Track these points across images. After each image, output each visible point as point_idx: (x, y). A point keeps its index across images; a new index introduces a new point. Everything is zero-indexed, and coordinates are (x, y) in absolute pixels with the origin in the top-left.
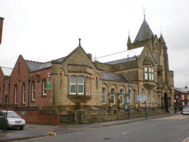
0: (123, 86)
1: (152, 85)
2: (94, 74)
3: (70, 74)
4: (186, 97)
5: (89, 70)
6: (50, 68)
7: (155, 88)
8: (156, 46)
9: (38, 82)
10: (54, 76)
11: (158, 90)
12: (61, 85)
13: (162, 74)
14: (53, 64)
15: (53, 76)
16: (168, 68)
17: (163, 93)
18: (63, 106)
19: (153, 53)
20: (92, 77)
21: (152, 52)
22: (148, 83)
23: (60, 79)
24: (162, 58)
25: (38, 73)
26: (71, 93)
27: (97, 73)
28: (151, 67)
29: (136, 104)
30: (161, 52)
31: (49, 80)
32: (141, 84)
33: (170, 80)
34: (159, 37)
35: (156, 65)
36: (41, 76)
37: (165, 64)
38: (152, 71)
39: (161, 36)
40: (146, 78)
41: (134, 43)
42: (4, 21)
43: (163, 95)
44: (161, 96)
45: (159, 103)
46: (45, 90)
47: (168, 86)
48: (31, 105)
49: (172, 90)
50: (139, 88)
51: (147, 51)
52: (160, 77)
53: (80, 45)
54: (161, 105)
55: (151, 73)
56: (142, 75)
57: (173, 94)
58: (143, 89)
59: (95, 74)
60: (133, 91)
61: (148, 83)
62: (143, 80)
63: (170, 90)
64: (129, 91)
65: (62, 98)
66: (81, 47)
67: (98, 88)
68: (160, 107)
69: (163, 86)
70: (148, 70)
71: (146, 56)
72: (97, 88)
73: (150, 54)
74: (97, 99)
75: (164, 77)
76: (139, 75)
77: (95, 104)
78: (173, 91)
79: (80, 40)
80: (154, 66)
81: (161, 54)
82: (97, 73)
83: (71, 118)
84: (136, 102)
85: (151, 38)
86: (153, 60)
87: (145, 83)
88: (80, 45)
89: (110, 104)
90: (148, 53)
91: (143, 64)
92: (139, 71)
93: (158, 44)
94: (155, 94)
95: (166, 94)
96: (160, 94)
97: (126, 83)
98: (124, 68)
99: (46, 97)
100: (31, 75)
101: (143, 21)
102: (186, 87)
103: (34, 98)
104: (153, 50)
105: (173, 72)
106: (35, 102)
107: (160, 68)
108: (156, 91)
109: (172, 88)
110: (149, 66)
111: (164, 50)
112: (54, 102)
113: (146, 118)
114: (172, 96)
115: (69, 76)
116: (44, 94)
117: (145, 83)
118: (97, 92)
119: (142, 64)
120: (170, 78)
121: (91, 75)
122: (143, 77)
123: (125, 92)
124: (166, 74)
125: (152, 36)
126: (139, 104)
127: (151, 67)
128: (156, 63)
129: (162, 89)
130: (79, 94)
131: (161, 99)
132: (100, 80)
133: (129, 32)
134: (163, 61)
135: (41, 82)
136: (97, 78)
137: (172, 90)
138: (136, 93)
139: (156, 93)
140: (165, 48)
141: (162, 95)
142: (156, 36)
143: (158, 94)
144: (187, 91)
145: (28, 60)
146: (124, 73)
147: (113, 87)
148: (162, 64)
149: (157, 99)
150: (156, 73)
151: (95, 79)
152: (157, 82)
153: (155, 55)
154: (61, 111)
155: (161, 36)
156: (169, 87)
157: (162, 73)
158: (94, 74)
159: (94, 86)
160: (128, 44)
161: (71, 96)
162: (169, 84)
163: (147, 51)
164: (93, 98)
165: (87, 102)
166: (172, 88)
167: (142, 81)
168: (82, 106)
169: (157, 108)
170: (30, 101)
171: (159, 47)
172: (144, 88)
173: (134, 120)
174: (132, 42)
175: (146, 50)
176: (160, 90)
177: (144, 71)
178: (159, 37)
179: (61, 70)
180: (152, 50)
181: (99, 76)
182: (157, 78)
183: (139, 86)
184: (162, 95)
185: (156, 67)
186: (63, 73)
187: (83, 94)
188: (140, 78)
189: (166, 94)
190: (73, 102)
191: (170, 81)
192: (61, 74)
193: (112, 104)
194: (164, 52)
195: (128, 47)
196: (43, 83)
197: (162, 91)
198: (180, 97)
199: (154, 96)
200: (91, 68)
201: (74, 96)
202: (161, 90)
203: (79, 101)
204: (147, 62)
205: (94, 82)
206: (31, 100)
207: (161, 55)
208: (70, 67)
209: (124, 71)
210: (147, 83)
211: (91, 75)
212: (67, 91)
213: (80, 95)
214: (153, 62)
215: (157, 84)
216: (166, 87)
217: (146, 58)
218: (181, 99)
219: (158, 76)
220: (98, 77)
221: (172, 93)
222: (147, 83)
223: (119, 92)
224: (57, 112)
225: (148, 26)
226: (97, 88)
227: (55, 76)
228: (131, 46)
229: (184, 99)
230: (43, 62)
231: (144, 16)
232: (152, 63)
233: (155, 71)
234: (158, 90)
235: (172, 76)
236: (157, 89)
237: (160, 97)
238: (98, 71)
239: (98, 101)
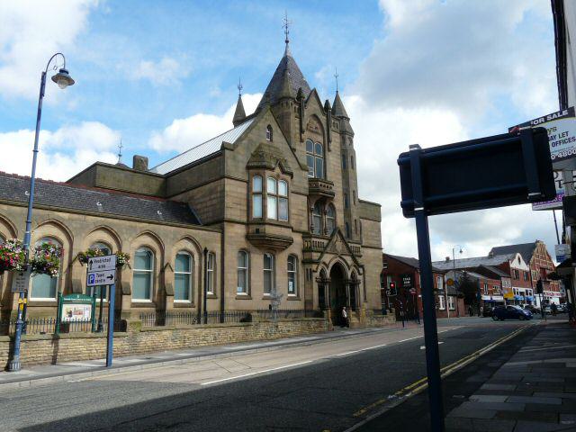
11: (307, 256)
13: (333, 208)
16: (355, 192)
17: (324, 263)
24: (334, 161)
28: (277, 179)
29: (208, 301)
30: (329, 141)
40: (257, 212)
43: (328, 272)
44: (317, 275)
50: (226, 245)
55: (276, 196)
56: (245, 203)
58: (243, 252)
60: (200, 255)
62: (245, 220)
68: (312, 311)
70: (264, 187)
76: (228, 201)
81: (332, 147)
84: (209, 293)
90: (270, 136)
91: (248, 168)
93: (323, 119)
97: (166, 225)
101: (281, 56)
104: (302, 131)
110: (268, 173)
117: (253, 228)
119: (242, 166)
120: (366, 223)
122: (245, 208)
127: (278, 176)
140: (346, 134)
142: (315, 93)
143: (308, 266)
145: (15, 173)
156: (347, 246)
163: (269, 127)
167: (243, 223)
169: (303, 314)
171: (325, 127)
177: (249, 189)
183: (226, 239)
188: (233, 211)
189: (338, 269)
197: (320, 258)
207: (329, 150)
210: (257, 231)
217: (260, 147)
222: (257, 231)
231: (287, 42)
234: (307, 256)
236: (304, 251)
237: (314, 280)
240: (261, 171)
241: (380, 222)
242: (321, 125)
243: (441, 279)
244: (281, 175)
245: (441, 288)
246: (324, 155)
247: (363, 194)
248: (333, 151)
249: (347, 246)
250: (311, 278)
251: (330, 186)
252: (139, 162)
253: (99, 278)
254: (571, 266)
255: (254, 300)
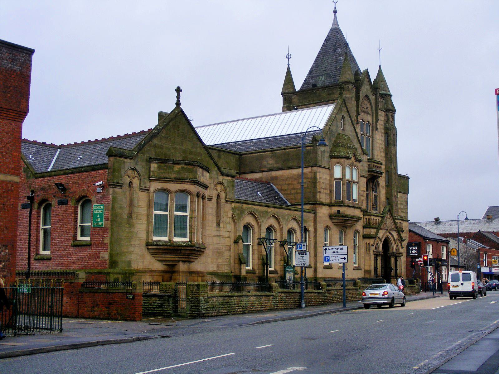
0: (274, 216)
1: (352, 217)
2: (212, 186)
3: (154, 186)
4: (437, 251)
5: (203, 175)
6: (101, 169)
7: (359, 226)
8: (366, 104)
9: (61, 203)
10: (113, 190)
11: (367, 231)
12: (130, 215)
14: (112, 159)
15: (111, 190)
16: (396, 168)
17: (379, 238)
18: (135, 270)
19: (358, 123)
20: (207, 193)
21: (353, 119)
22: (342, 210)
23: (128, 199)
24: (379, 139)
25: (63, 179)
26: (156, 238)
27: (221, 183)
28: (351, 166)
30: (377, 121)
31: (99, 202)
32: (323, 212)
33: (399, 202)
34: (373, 76)
35: (365, 158)
36: (73, 189)
37: (386, 154)
38: (355, 178)
39: (380, 73)
41: (301, 91)
42: (35, 57)
43: (381, 245)
44: (373, 248)
45: (367, 268)
46: (83, 228)
47: (394, 219)
48: (37, 267)
49: (403, 231)
50: (318, 225)
51: (343, 118)
52: (373, 194)
53: (178, 104)
54: (373, 273)
57: (405, 243)
58: (327, 228)
59: (215, 185)
61: (342, 210)
63: (399, 231)
64: (290, 232)
65: (131, 249)
66: (182, 111)
67: (222, 225)
69: (380, 219)
71: (338, 134)
72: (218, 224)
73: (349, 128)
74: (219, 253)
75: (382, 193)
77: (212, 268)
78: (405, 235)
79: (178, 90)
80: (360, 161)
81: (378, 126)
82: (221, 183)
83: (169, 302)
85: (354, 81)
86: (357, 145)
87: (335, 209)
88: (178, 104)
89: (240, 269)
91: (331, 157)
92: (318, 176)
93: (372, 98)
94: (359, 239)
95: (386, 243)
96: (371, 241)
98: (275, 166)
99: (87, 245)
100: (38, 183)
101: (329, 27)
102: (437, 221)
103: (45, 249)
104: (358, 114)
105: (407, 178)
106: (50, 259)
107: (375, 169)
108: (361, 233)
109: (405, 224)
110: (347, 161)
111: (387, 115)
112: (113, 264)
113: (434, 295)
114: (402, 248)
115: (152, 190)
116: (80, 238)
117: (335, 209)
118: (219, 236)
121: (206, 187)
122: (328, 192)
123: (278, 234)
124: (389, 185)
125: (357, 73)
126: (315, 271)
127: (353, 163)
128: (364, 153)
129: (377, 228)
130: (176, 239)
131: (373, 257)
132: (227, 201)
133: (289, 57)
134: (383, 147)
135: (71, 203)
136: (218, 196)
137: (403, 231)
138: (309, 238)
139: (361, 238)
140: (390, 111)
141: (377, 244)
142: (367, 73)
143: (367, 241)
144: (438, 233)
145: (35, 139)
146: (276, 178)
147: (249, 219)
148: (379, 156)
149: (362, 255)
150: (364, 181)
151: (214, 199)
152: (364, 206)
153: (362, 130)
154: (118, 282)
155: (380, 73)
156: (395, 223)
157: (378, 182)
158: (212, 186)
159: (211, 218)
160: (286, 91)
161: (156, 245)
162: (395, 216)
163: (343, 118)
164: (208, 252)
165: (192, 262)
166: (405, 224)
168: (183, 272)
170: (33, 256)
171: (374, 106)
172: (330, 223)
173: (316, 310)
174: (298, 86)
175: (339, 117)
176: (373, 231)
178: (373, 76)
179: (130, 173)
180: (354, 114)
181: (225, 193)
182: (365, 195)
183: (318, 219)
184: (377, 244)
185: (364, 166)
186: (136, 182)
187: (186, 239)
189: (386, 243)
190: (158, 260)
191: (399, 206)
192: (130, 184)
193: (247, 268)
194: (387, 121)
195: (285, 100)
196: (76, 208)
197: (377, 233)
198: (421, 251)
199: (355, 247)
200: (207, 170)
201: (163, 245)
202: (375, 230)
203: (177, 259)
204: (341, 149)
205: (211, 207)
206: (37, 254)
207: (377, 130)
208: (154, 166)
209: (274, 174)
210: (339, 211)
211: (206, 187)
212: (145, 232)
213: (180, 244)
214: (356, 149)
215: (365, 212)
216: (389, 220)
218: (425, 258)
219: (367, 190)
220: (223, 195)
221: (403, 240)
222: (339, 211)
223: (263, 235)
224: (138, 288)
225: (346, 45)
226: (218, 224)
227: (118, 190)
228: (295, 99)
229: (431, 257)
230: (58, 144)
231: (335, 12)
232: (354, 155)
233: (361, 176)
234: (367, 231)
235: (406, 191)
236: (364, 227)
238: (221, 178)
239: (220, 261)
240: (342, 160)
241: (408, 193)
242: (371, 105)
243: (445, 249)
244: (355, 163)
245: (444, 257)
246: (372, 134)
247: (401, 171)
248: (379, 130)
249: (395, 223)
250: (369, 250)
251: (379, 165)
252: (161, 115)
253: (333, 259)
254: (441, 284)
255: (334, 269)
